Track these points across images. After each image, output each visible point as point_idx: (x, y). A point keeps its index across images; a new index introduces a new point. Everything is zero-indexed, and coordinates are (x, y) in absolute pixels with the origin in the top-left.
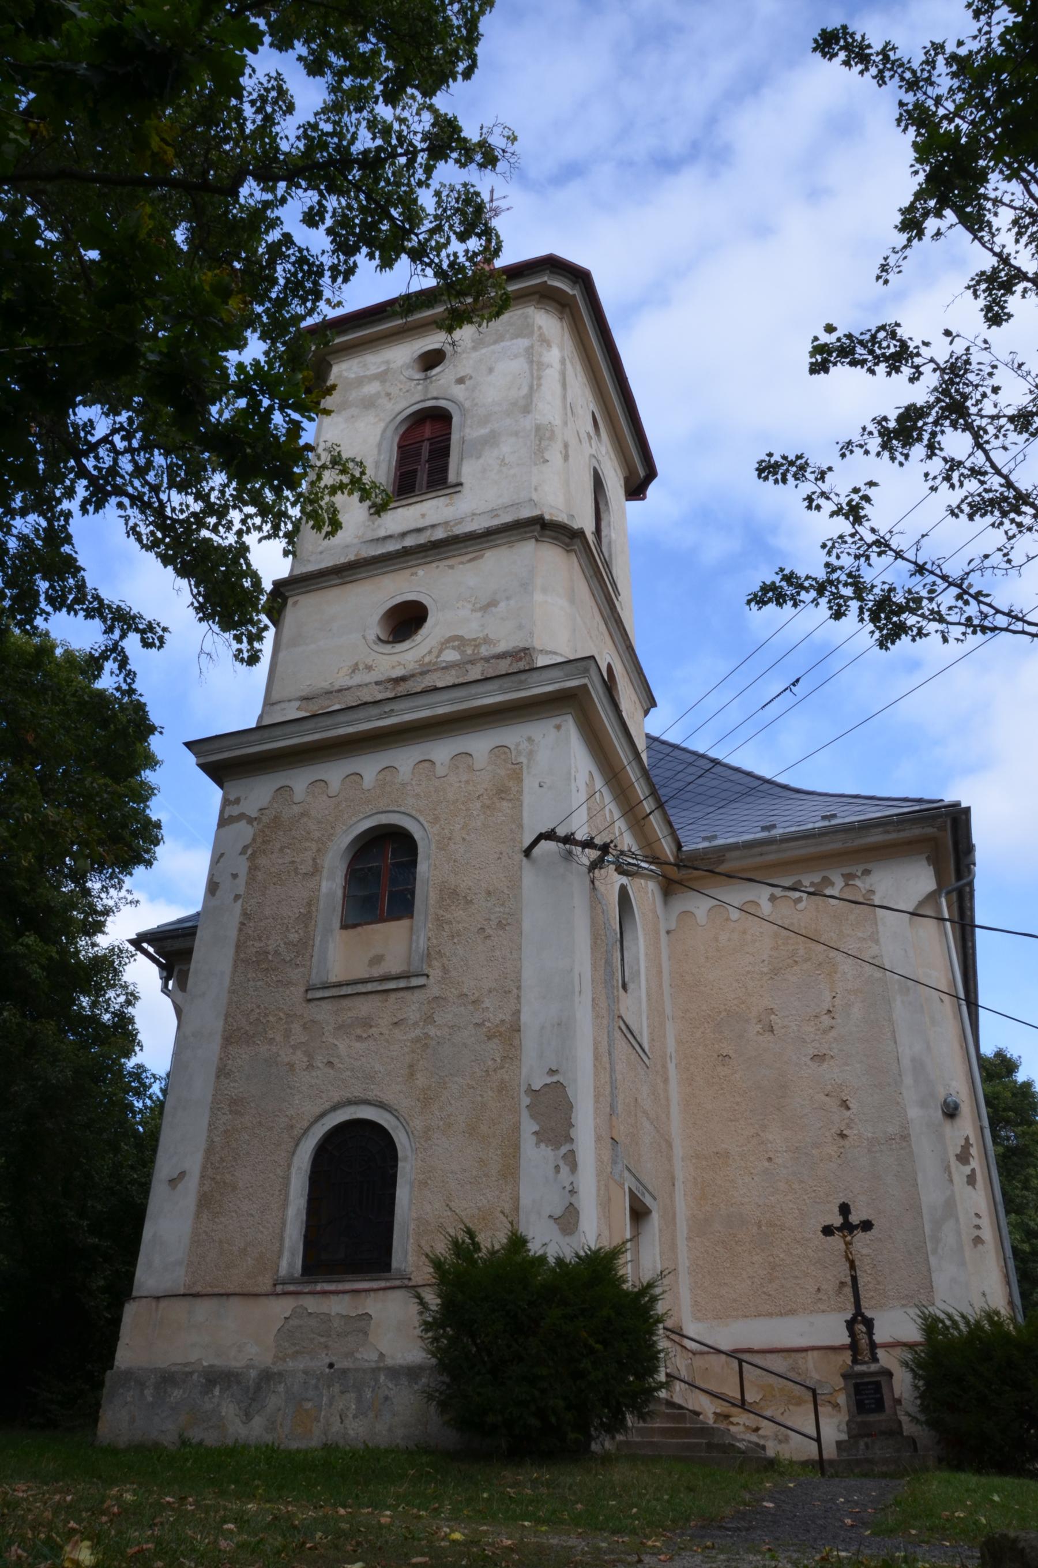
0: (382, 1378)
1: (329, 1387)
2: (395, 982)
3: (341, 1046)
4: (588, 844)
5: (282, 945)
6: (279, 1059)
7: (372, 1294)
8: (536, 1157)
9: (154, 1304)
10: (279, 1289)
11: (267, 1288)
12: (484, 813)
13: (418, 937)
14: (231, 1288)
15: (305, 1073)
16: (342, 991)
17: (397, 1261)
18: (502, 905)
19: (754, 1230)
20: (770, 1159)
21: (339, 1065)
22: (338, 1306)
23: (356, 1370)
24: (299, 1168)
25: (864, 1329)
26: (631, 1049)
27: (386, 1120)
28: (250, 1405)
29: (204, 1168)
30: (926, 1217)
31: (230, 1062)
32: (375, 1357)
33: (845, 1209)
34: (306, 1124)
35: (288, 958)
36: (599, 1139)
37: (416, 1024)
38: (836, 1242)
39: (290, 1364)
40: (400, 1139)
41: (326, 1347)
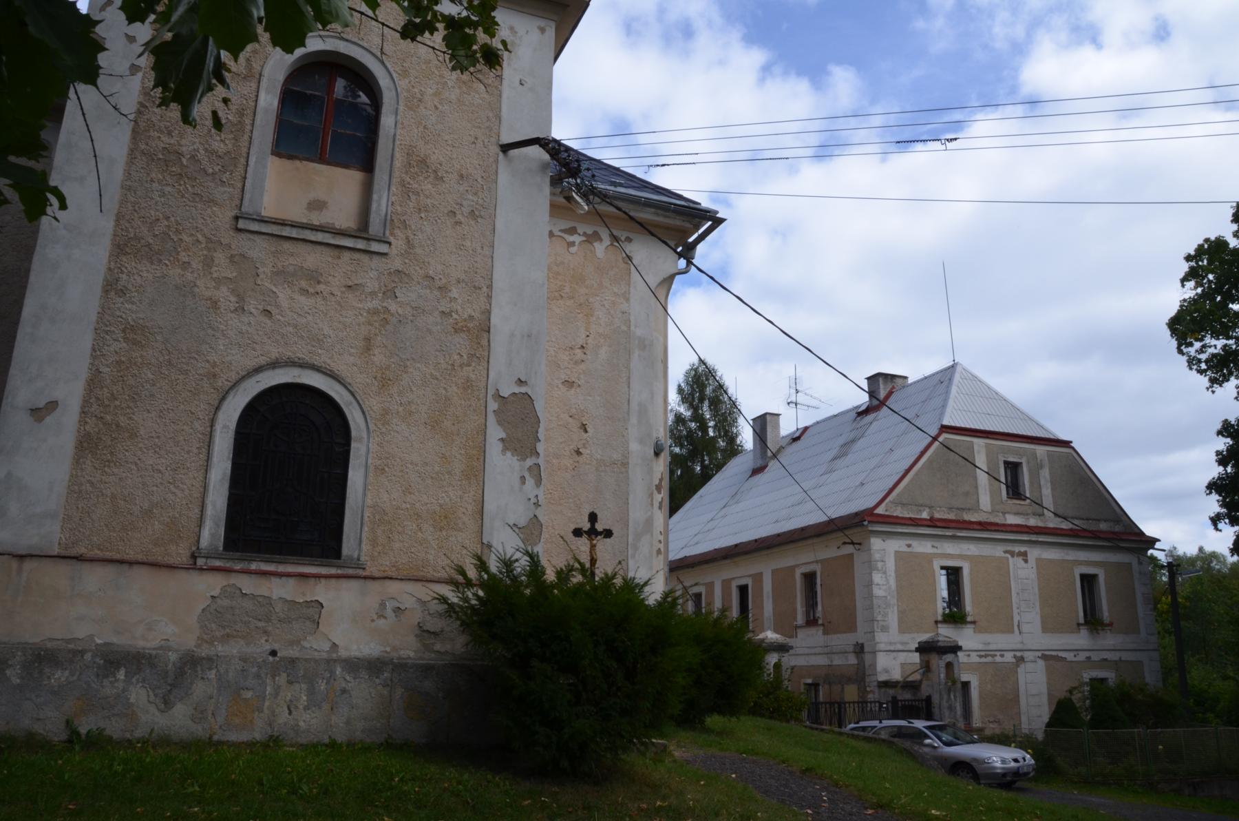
0: (339, 671)
1: (273, 677)
2: (352, 240)
3: (281, 295)
5: (202, 152)
6: (196, 290)
7: (323, 580)
8: (502, 466)
9: (14, 564)
12: (460, 88)
13: (380, 198)
14: (131, 555)
15: (233, 315)
16: (283, 232)
17: (348, 548)
18: (476, 194)
21: (279, 317)
22: (281, 590)
23: (306, 660)
24: (225, 427)
27: (337, 393)
28: (170, 691)
29: (86, 403)
30: (631, 530)
31: (124, 277)
32: (326, 646)
33: (593, 517)
34: (234, 377)
35: (211, 171)
37: (373, 294)
39: (220, 649)
40: (354, 416)
41: (265, 632)
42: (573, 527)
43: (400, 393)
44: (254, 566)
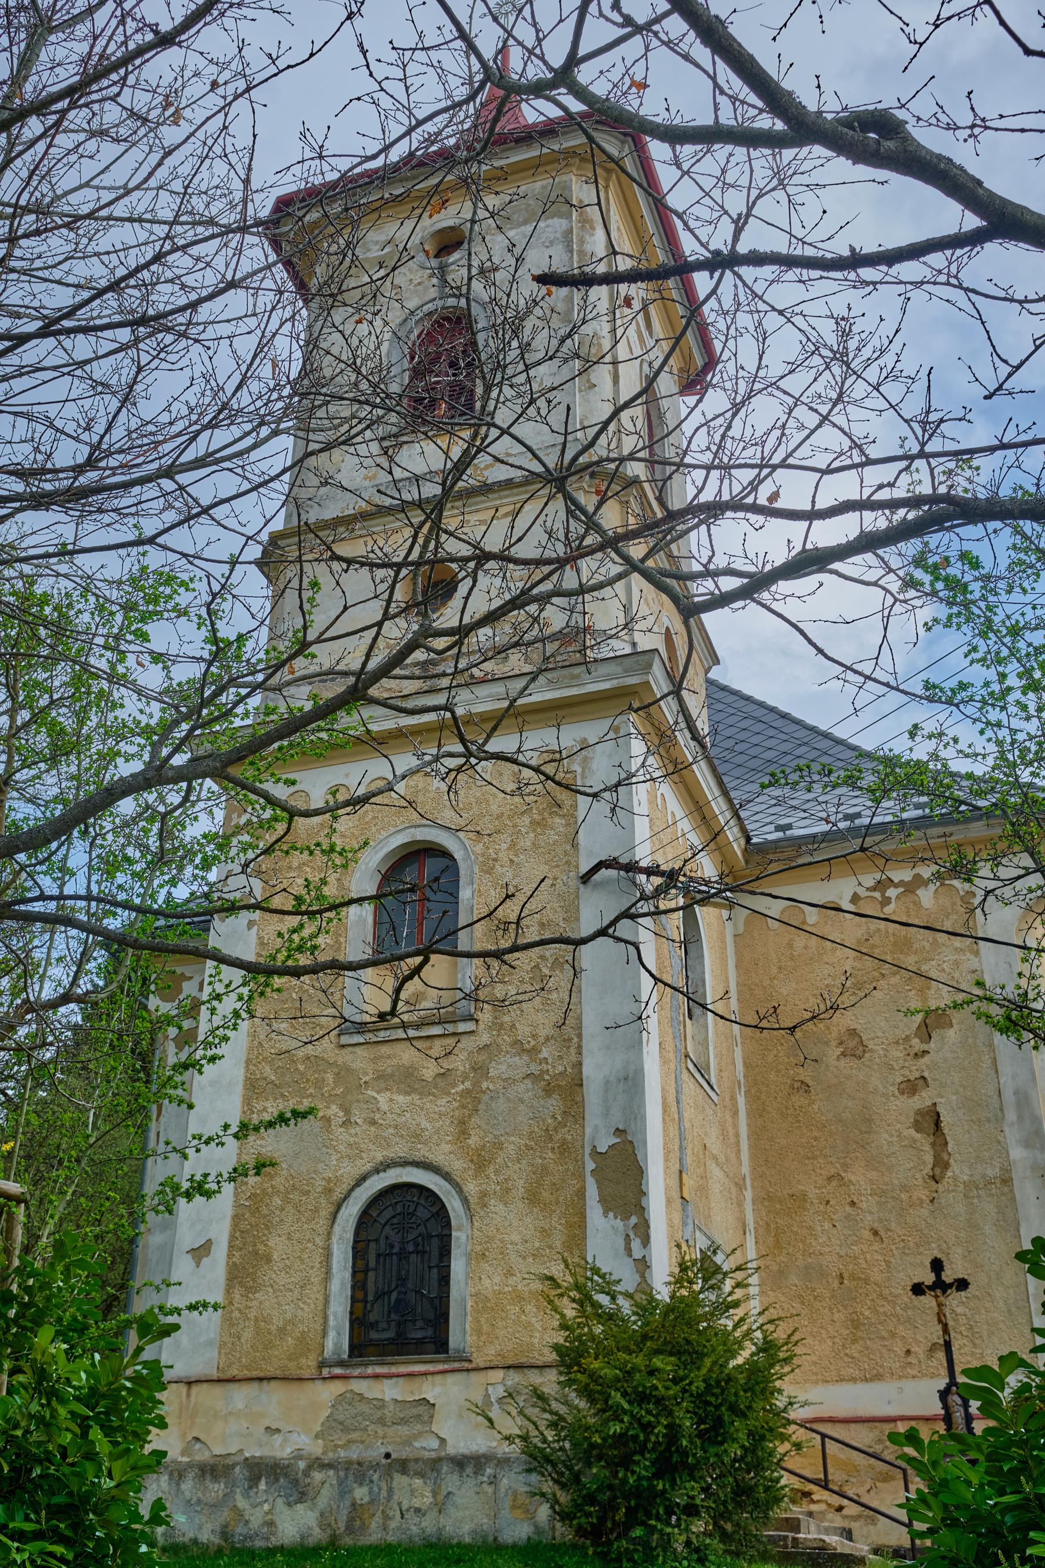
4: (650, 872)
10: (325, 1372)
11: (312, 1372)
14: (271, 1370)
17: (454, 1341)
19: (836, 1284)
20: (853, 1204)
22: (390, 1391)
23: (416, 1460)
25: (959, 1401)
26: (699, 1090)
29: (232, 1238)
33: (937, 1265)
36: (669, 1201)
38: (928, 1301)
40: (454, 1205)
42: (909, 1285)
43: (497, 1172)
44: (370, 1370)
